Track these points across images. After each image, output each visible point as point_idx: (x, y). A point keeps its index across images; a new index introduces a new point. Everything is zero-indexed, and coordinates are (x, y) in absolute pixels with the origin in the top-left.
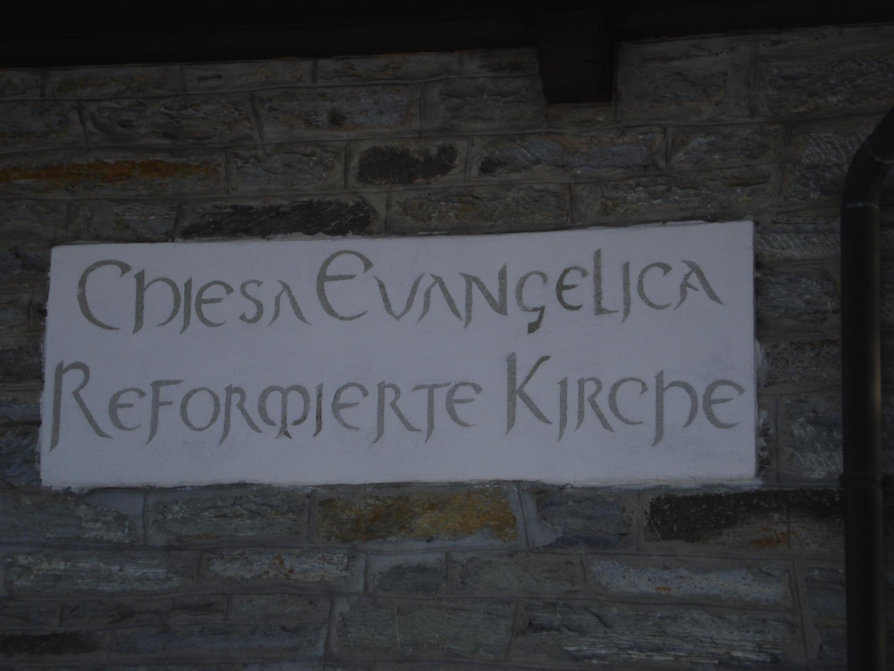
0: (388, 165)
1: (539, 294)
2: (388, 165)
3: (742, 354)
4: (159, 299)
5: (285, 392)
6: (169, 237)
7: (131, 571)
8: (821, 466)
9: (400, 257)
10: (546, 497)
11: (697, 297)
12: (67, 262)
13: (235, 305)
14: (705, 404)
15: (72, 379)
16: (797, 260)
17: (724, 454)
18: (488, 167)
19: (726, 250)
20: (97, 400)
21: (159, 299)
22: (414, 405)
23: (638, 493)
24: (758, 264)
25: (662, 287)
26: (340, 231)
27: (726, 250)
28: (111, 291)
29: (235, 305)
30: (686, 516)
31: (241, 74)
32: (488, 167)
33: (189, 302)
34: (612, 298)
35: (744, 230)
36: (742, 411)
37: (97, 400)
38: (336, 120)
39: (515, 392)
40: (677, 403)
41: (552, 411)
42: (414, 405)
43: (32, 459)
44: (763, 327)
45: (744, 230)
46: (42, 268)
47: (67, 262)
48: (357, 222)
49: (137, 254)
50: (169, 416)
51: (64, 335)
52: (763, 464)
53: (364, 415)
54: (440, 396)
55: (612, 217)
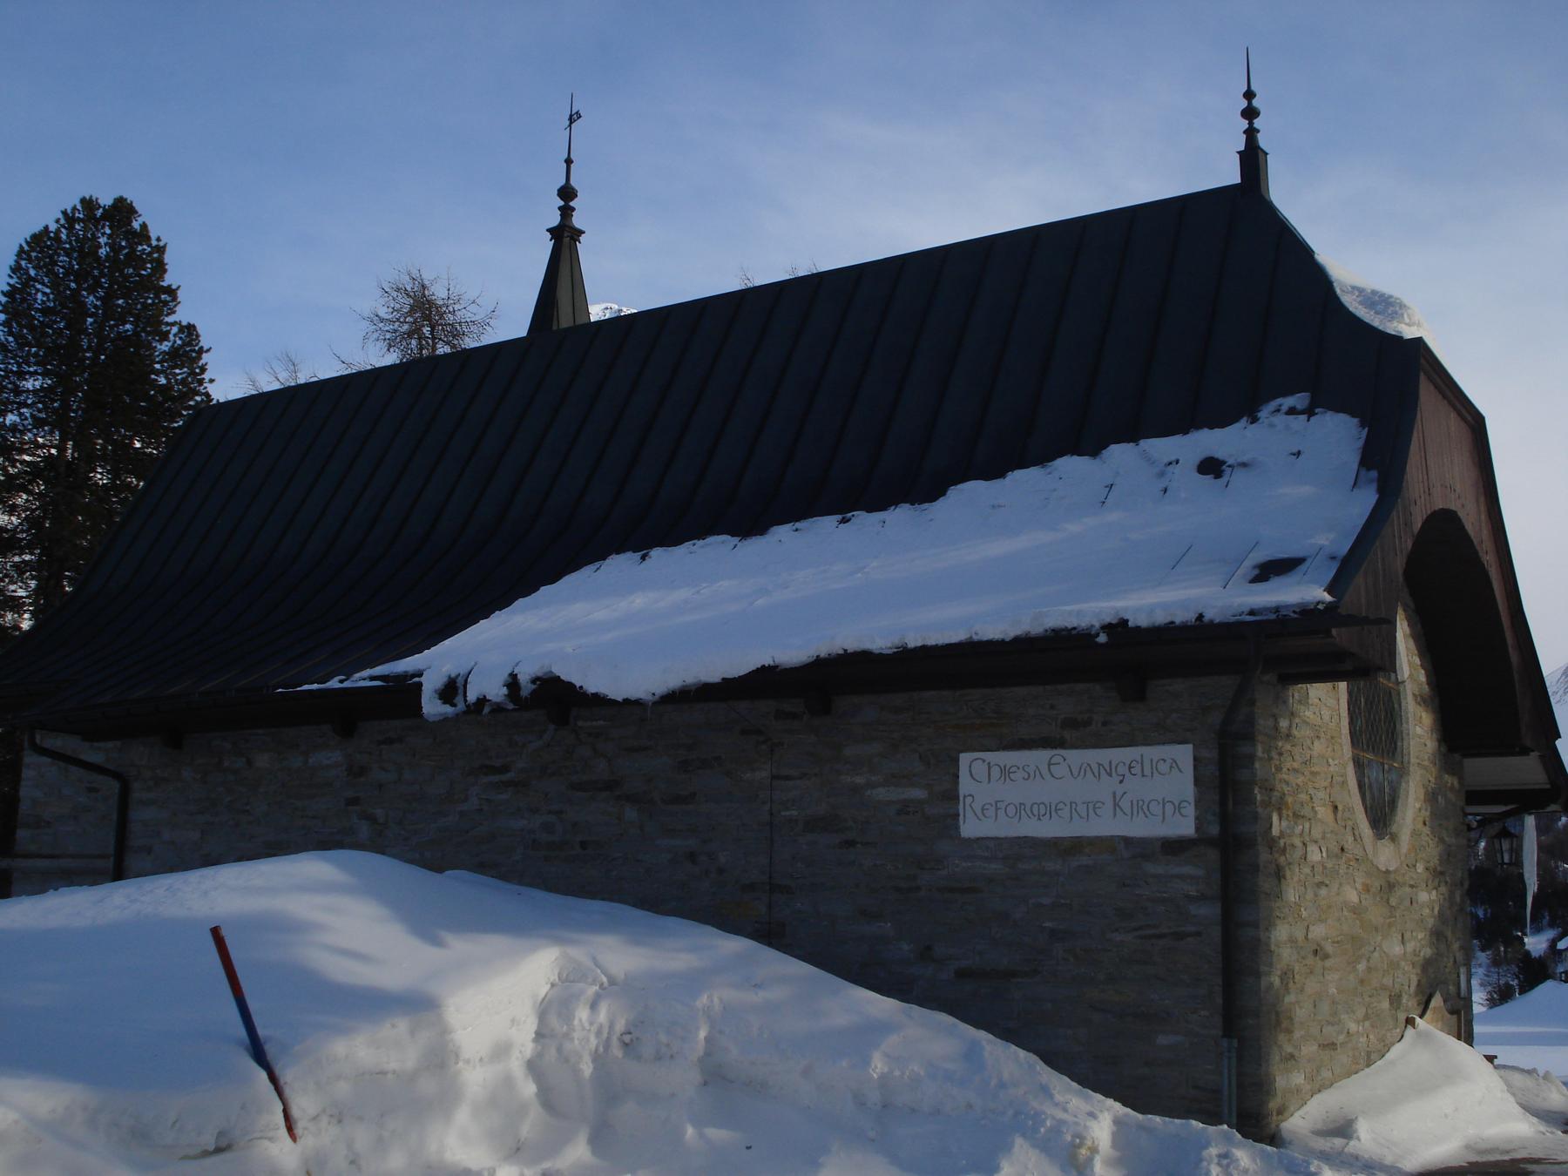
0: (1071, 723)
1: (1122, 770)
2: (1071, 723)
3: (1188, 790)
4: (995, 772)
5: (1466, 814)
6: (998, 750)
7: (993, 866)
8: (1214, 830)
9: (1075, 757)
10: (1127, 841)
11: (1175, 770)
12: (965, 758)
13: (1020, 775)
14: (1178, 808)
15: (969, 800)
16: (1459, 414)
17: (1185, 826)
18: (1105, 724)
19: (1184, 754)
20: (977, 807)
21: (995, 772)
22: (1082, 809)
23: (1157, 839)
24: (1195, 759)
25: (1163, 767)
26: (1055, 747)
27: (1184, 754)
28: (980, 769)
29: (1020, 775)
30: (1173, 847)
31: (1021, 691)
32: (1105, 724)
33: (1006, 772)
34: (1147, 771)
35: (1190, 746)
36: (1190, 811)
37: (977, 807)
38: (1052, 707)
39: (1116, 805)
40: (1169, 808)
41: (1128, 811)
42: (1082, 809)
43: (957, 828)
44: (1197, 782)
45: (1190, 746)
46: (957, 760)
47: (965, 758)
48: (1061, 744)
49: (988, 756)
50: (1001, 813)
51: (965, 785)
52: (1197, 829)
53: (1066, 812)
54: (1169, 808)
55: (1147, 742)
